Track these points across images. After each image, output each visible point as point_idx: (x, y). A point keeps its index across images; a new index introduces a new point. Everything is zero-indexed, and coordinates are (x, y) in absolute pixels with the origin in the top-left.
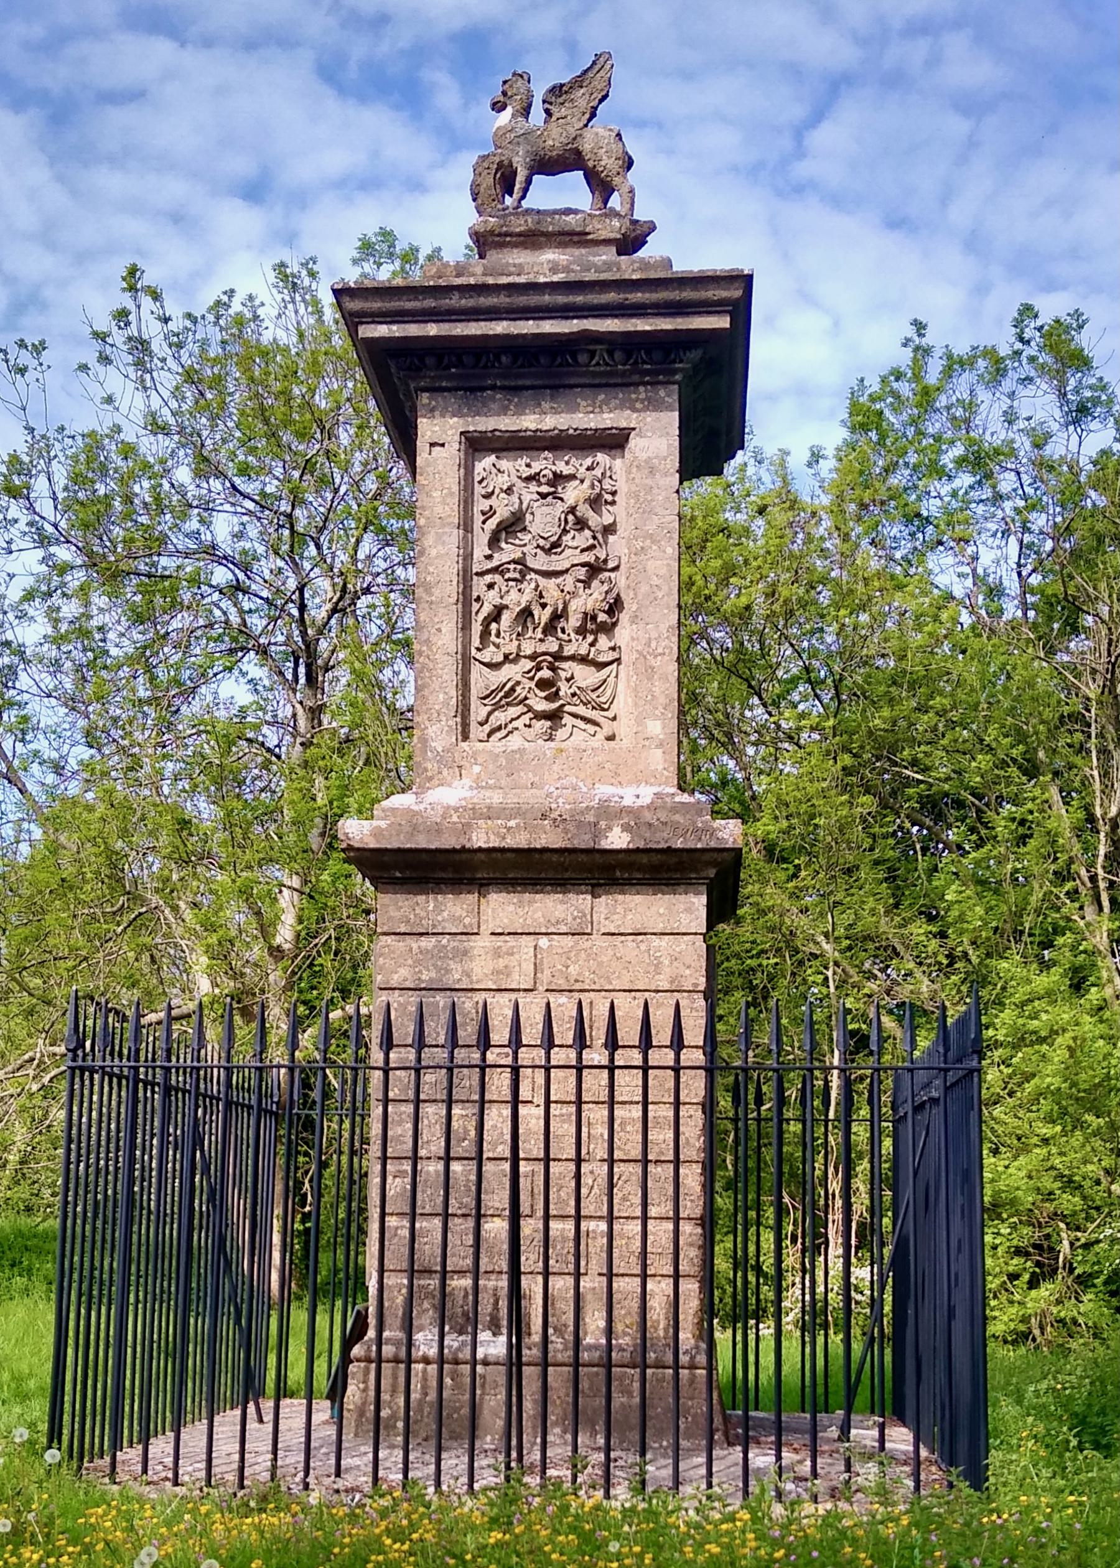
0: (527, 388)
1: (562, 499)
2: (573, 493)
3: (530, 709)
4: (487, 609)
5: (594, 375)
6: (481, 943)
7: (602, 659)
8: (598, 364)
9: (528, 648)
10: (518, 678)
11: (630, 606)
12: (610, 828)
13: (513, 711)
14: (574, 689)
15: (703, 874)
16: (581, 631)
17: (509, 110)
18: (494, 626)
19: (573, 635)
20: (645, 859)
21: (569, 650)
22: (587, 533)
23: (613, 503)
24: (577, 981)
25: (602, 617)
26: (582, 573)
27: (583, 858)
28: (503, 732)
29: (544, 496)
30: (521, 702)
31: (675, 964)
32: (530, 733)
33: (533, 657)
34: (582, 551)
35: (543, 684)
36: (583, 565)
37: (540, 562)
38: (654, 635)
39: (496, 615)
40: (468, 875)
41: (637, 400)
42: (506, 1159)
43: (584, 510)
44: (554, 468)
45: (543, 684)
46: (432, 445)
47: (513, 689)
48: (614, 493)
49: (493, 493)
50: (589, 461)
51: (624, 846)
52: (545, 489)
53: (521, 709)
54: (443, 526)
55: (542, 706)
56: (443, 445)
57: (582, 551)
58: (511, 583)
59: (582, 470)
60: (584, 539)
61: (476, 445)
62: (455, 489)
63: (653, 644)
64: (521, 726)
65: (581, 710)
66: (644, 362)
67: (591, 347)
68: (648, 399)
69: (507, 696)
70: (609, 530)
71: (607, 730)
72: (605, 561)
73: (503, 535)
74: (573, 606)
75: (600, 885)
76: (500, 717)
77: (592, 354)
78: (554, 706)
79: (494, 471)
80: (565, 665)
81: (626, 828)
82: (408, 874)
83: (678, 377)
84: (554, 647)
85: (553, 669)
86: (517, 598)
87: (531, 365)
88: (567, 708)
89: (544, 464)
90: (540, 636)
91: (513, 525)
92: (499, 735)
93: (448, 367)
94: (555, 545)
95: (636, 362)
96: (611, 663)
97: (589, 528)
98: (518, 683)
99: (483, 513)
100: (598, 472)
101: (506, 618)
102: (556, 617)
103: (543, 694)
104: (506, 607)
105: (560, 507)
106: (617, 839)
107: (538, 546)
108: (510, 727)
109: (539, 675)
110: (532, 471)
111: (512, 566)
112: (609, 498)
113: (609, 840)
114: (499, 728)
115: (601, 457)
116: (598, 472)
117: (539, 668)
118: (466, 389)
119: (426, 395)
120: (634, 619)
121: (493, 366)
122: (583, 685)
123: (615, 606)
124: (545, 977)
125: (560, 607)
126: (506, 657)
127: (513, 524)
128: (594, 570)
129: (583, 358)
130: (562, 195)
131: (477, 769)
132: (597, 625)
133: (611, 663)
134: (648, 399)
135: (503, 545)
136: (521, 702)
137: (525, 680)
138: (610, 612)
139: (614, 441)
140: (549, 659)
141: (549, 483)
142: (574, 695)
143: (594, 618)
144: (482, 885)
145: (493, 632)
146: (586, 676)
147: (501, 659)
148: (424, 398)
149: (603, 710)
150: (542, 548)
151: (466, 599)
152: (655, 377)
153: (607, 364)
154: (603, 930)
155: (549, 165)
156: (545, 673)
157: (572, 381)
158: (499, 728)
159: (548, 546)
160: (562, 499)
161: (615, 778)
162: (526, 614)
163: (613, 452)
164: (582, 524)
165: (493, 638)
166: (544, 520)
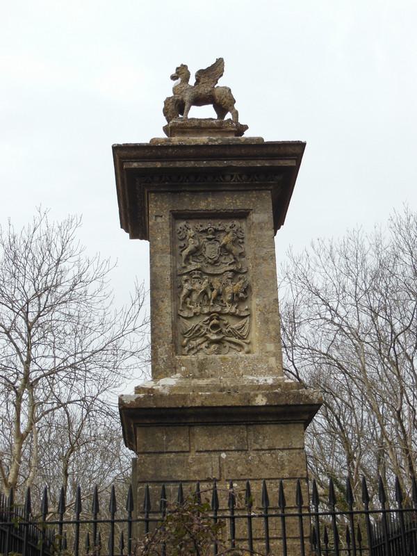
0: (201, 191)
1: (219, 241)
2: (224, 239)
3: (208, 339)
4: (185, 291)
5: (233, 185)
6: (192, 456)
7: (242, 314)
8: (234, 181)
9: (206, 310)
10: (201, 324)
11: (255, 290)
12: (257, 395)
13: (199, 341)
14: (229, 329)
15: (302, 418)
16: (232, 302)
17: (180, 79)
18: (188, 299)
19: (227, 303)
20: (274, 410)
21: (227, 310)
22: (231, 256)
23: (243, 242)
24: (241, 475)
25: (241, 295)
26: (230, 275)
27: (244, 410)
28: (195, 350)
29: (210, 239)
30: (203, 336)
31: (291, 464)
32: (208, 351)
33: (209, 314)
34: (230, 264)
35: (215, 327)
36: (231, 271)
37: (210, 270)
38: (267, 303)
39: (191, 292)
40: (184, 421)
41: (252, 197)
42: (263, 539)
43: (229, 246)
44: (214, 227)
45: (215, 327)
46: (156, 216)
47: (199, 330)
48: (243, 239)
49: (185, 238)
50: (230, 224)
51: (264, 404)
52: (211, 236)
53: (202, 339)
54: (163, 253)
55: (214, 337)
56: (162, 216)
57: (230, 264)
58: (195, 280)
59: (228, 228)
60: (230, 259)
61: (177, 216)
62: (168, 236)
63: (267, 307)
64: (204, 347)
65: (233, 339)
66: (256, 180)
67: (232, 173)
68: (257, 197)
69: (196, 334)
70: (242, 255)
71: (246, 349)
72: (241, 269)
73: (191, 257)
74: (228, 289)
75: (250, 424)
76: (194, 343)
77: (232, 176)
78: (221, 336)
79: (186, 229)
80: (224, 318)
81: (266, 395)
82: (153, 421)
83: (271, 187)
84: (219, 309)
85: (218, 319)
86: (201, 286)
87: (204, 181)
88: (227, 338)
89: (207, 225)
90: (212, 304)
91: (196, 253)
92: (193, 352)
93: (164, 182)
94: (216, 262)
95: (252, 181)
96: (246, 316)
97: (232, 254)
98: (201, 327)
99: (181, 247)
100: (235, 229)
101: (195, 296)
102: (219, 295)
103: (215, 332)
104: (194, 290)
105: (218, 245)
106: (261, 401)
107: (208, 262)
108: (199, 348)
109: (212, 322)
110: (204, 228)
111: (196, 272)
112: (241, 240)
113: (256, 402)
114: (193, 348)
115: (236, 222)
116: (235, 229)
117: (211, 319)
118: (172, 192)
119: (153, 194)
120: (258, 295)
121: (186, 182)
122: (234, 327)
123: (247, 289)
124: (225, 474)
125: (221, 290)
126: (195, 314)
127: (195, 253)
128: (236, 273)
129: (228, 178)
130: (205, 112)
131: (183, 368)
132: (239, 299)
133: (246, 316)
134: (257, 197)
135: (191, 261)
136: (203, 336)
137: (204, 326)
138: (245, 292)
139: (243, 215)
140: (217, 315)
141: (213, 234)
142: (229, 332)
143: (237, 295)
144: (190, 426)
145: (188, 303)
146: (235, 324)
147: (192, 315)
148: (152, 196)
149: (244, 339)
150: (210, 263)
151: (177, 288)
152: (260, 188)
153: (238, 181)
154: (253, 448)
155: (199, 101)
156: (215, 321)
157: (223, 188)
158: (193, 348)
159: (213, 262)
160: (219, 241)
161: (254, 371)
162: (205, 293)
163: (241, 220)
164: (229, 252)
165: (188, 305)
166: (211, 251)
